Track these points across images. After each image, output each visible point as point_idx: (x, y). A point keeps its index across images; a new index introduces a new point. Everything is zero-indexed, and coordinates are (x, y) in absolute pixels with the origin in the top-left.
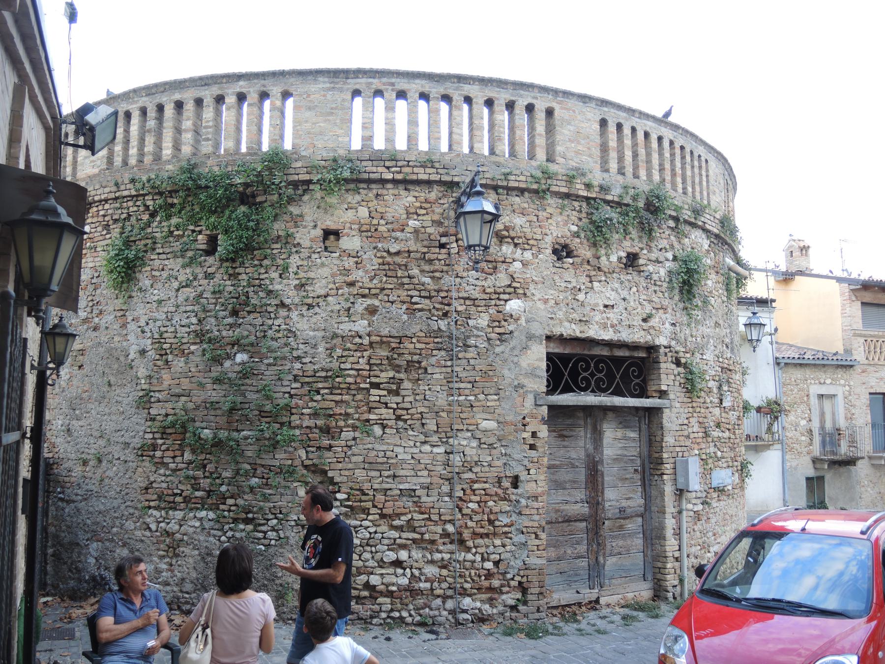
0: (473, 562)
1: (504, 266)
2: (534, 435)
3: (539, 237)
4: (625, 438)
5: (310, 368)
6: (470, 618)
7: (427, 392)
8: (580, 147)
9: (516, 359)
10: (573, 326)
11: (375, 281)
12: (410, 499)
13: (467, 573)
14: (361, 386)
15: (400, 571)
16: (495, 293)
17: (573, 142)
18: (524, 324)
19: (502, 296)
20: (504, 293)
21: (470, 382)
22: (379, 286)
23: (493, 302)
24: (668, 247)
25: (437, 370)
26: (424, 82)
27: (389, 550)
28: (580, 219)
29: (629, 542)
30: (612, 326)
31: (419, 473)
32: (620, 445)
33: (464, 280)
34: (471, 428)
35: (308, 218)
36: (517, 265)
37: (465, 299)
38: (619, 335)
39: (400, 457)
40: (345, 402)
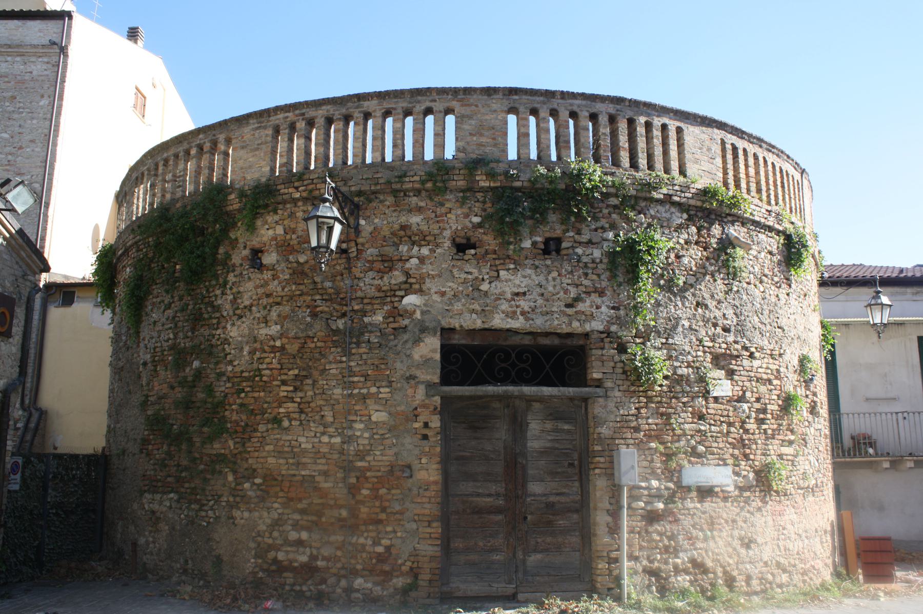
1: (400, 264)
2: (426, 425)
4: (556, 430)
5: (238, 369)
7: (326, 387)
8: (483, 140)
15: (301, 549)
17: (474, 135)
19: (398, 293)
20: (400, 290)
23: (389, 299)
24: (607, 226)
25: (334, 366)
26: (329, 107)
29: (560, 540)
30: (523, 313)
31: (318, 461)
32: (549, 438)
35: (241, 241)
36: (414, 261)
39: (303, 446)
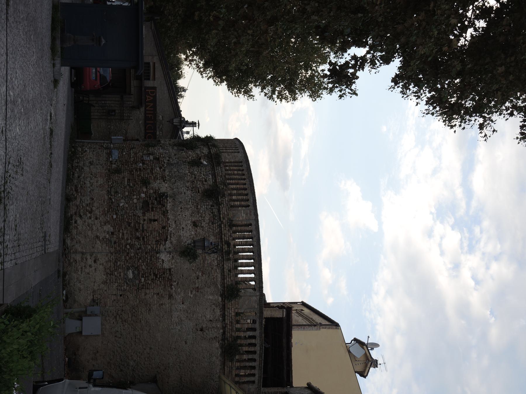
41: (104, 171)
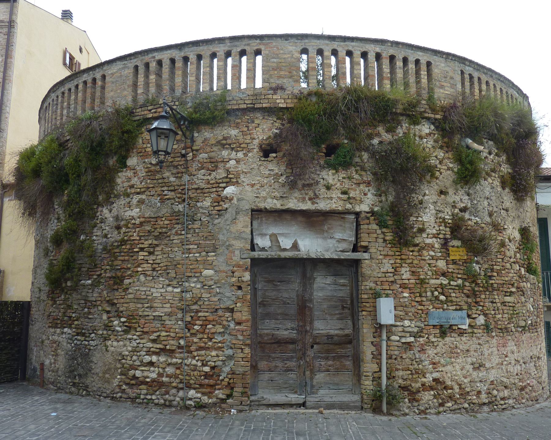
0: (196, 366)
3: (248, 141)
6: (193, 404)
7: (170, 252)
9: (228, 227)
10: (275, 201)
11: (143, 184)
12: (160, 322)
13: (192, 373)
14: (135, 250)
16: (217, 183)
17: (276, 70)
18: (236, 203)
19: (221, 185)
20: (223, 183)
21: (196, 244)
22: (145, 186)
25: (176, 237)
27: (147, 355)
28: (283, 125)
31: (164, 305)
33: (195, 177)
34: (197, 275)
36: (232, 162)
37: (196, 189)
38: (316, 205)
39: (154, 295)
40: (126, 260)
41: (494, 341)
